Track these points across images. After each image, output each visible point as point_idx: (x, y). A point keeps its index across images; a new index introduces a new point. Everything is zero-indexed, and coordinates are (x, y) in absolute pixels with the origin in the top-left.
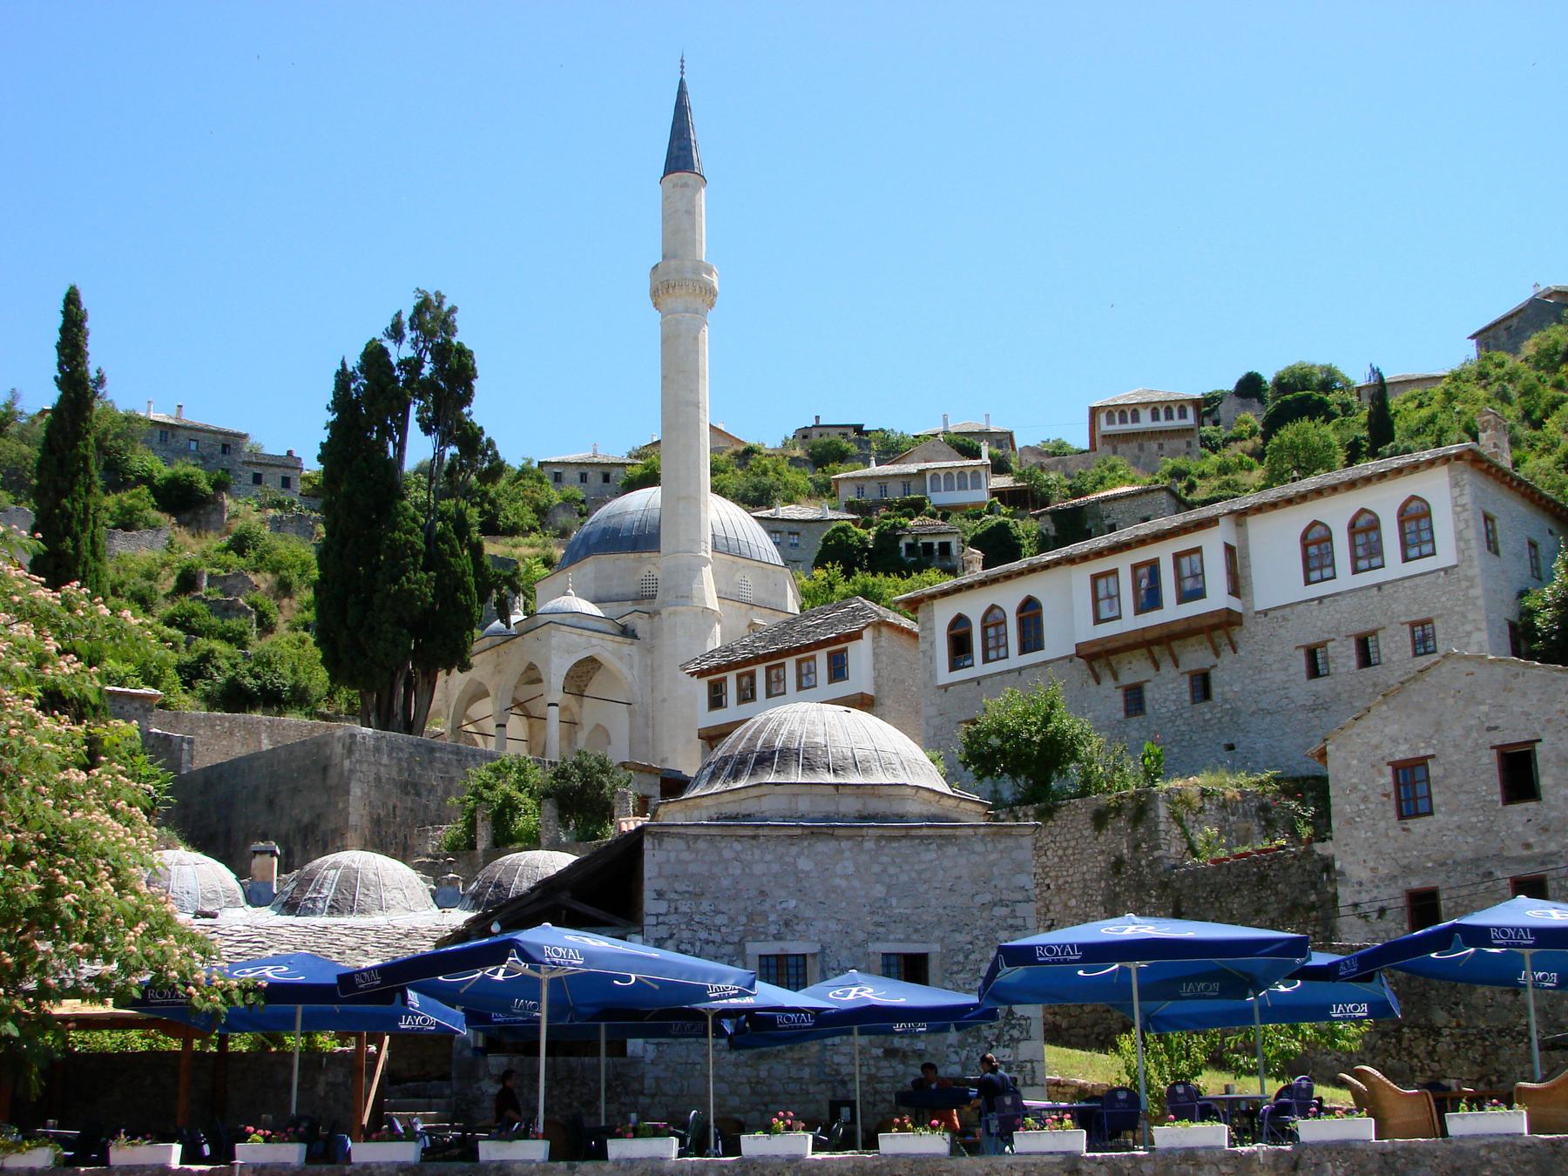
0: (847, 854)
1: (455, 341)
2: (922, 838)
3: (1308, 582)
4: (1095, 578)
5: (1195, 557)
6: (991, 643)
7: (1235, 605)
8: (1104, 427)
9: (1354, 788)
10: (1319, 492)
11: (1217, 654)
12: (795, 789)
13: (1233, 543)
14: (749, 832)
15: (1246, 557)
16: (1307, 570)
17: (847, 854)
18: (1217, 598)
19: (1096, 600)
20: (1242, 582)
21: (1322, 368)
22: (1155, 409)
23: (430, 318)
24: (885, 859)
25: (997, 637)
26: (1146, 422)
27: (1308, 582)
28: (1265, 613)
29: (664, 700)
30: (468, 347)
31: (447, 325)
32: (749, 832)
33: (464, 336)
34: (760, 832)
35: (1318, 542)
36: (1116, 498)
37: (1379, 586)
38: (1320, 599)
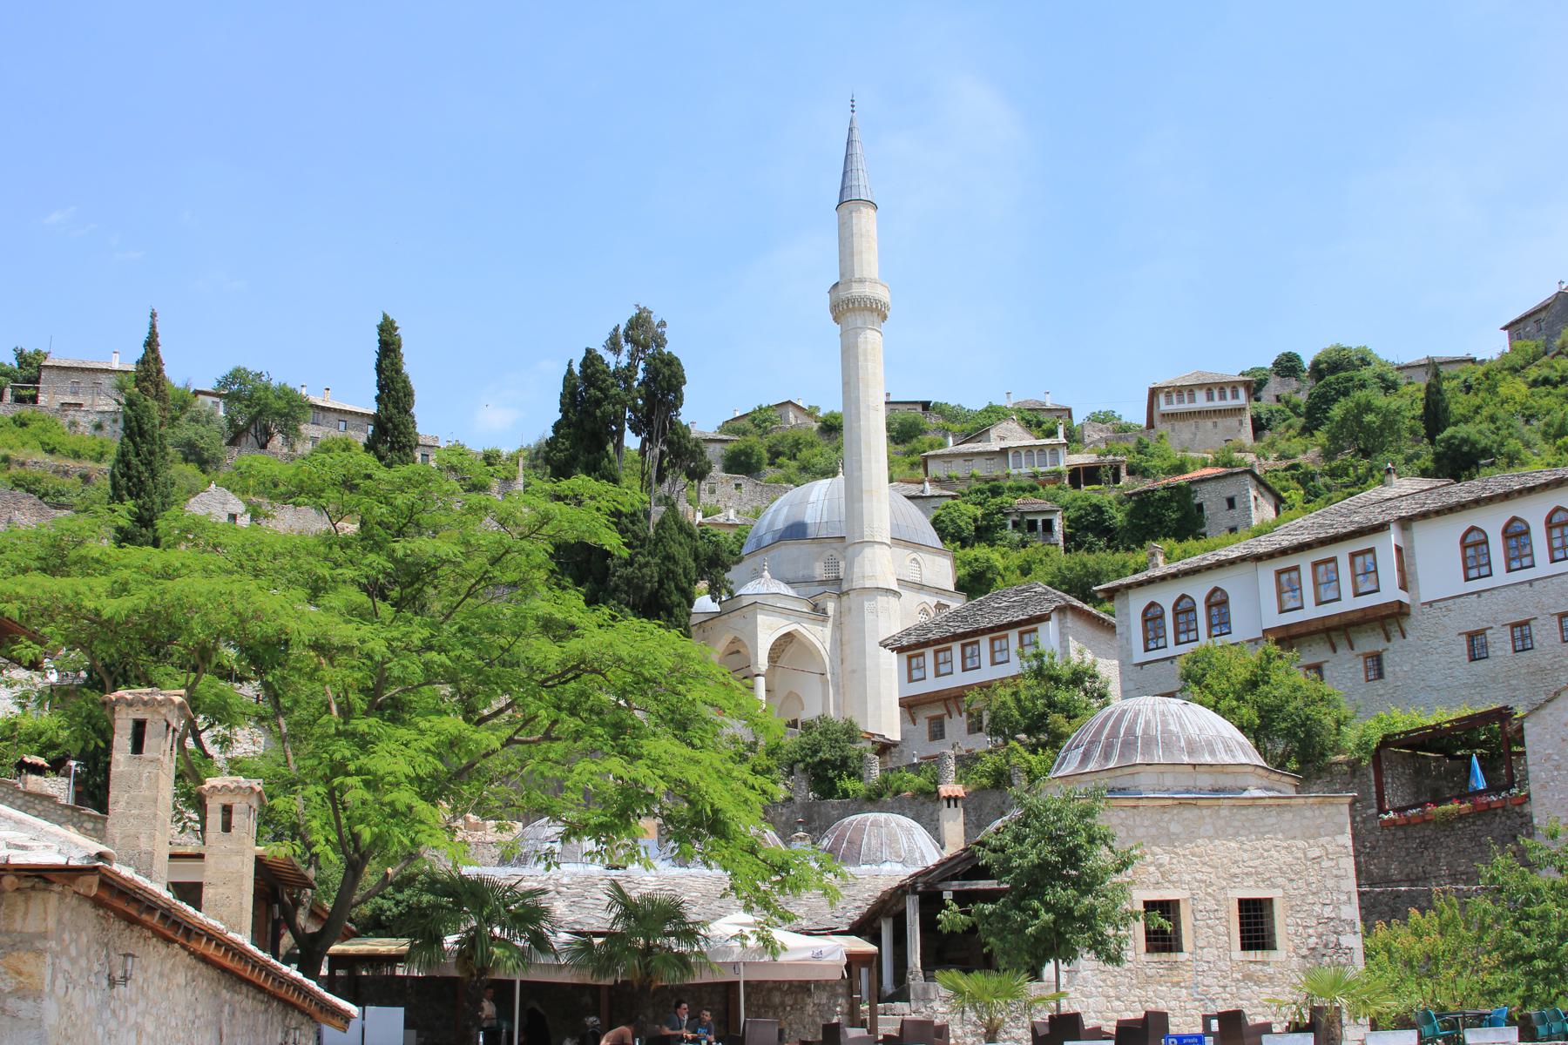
0: (1208, 820)
1: (665, 351)
2: (1265, 806)
3: (1467, 579)
4: (1279, 573)
5: (1369, 557)
6: (1182, 628)
7: (1404, 597)
8: (1163, 406)
9: (1549, 758)
10: (1478, 502)
11: (1389, 640)
12: (1162, 768)
13: (1401, 545)
14: (1132, 803)
15: (1412, 557)
16: (1466, 569)
17: (1208, 820)
18: (1390, 592)
19: (1280, 593)
20: (1409, 578)
21: (1357, 351)
22: (1209, 388)
23: (640, 332)
24: (1236, 824)
25: (1188, 622)
26: (1201, 402)
27: (1467, 579)
28: (1430, 604)
29: (853, 671)
30: (675, 354)
31: (660, 341)
32: (1132, 803)
33: (673, 346)
34: (1141, 803)
35: (1475, 545)
36: (1203, 480)
37: (1530, 582)
38: (1478, 593)
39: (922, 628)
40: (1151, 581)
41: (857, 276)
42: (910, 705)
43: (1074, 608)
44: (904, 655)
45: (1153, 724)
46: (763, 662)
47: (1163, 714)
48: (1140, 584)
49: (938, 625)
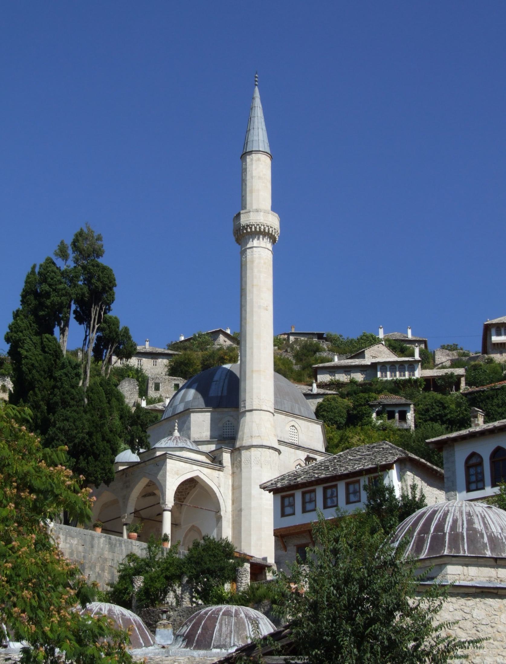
39: (296, 475)
40: (473, 436)
41: (254, 207)
42: (282, 537)
43: (412, 460)
44: (279, 496)
45: (460, 523)
46: (170, 500)
47: (469, 514)
48: (463, 438)
49: (307, 472)
